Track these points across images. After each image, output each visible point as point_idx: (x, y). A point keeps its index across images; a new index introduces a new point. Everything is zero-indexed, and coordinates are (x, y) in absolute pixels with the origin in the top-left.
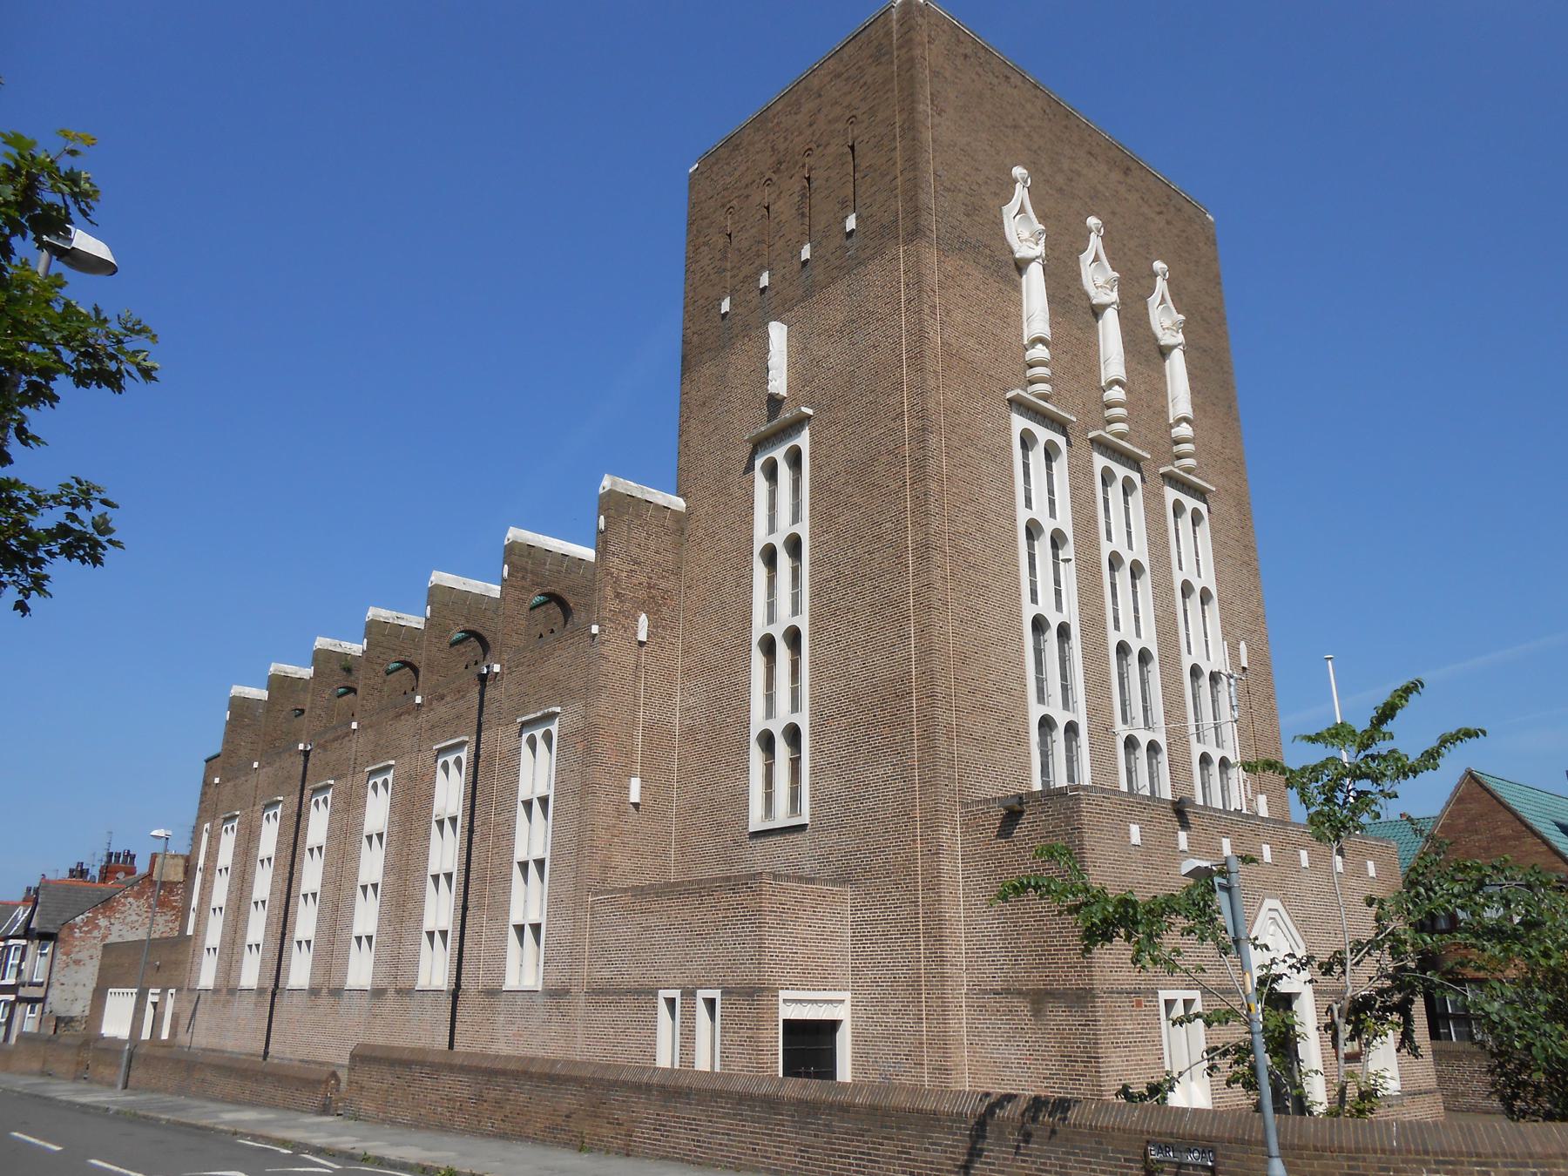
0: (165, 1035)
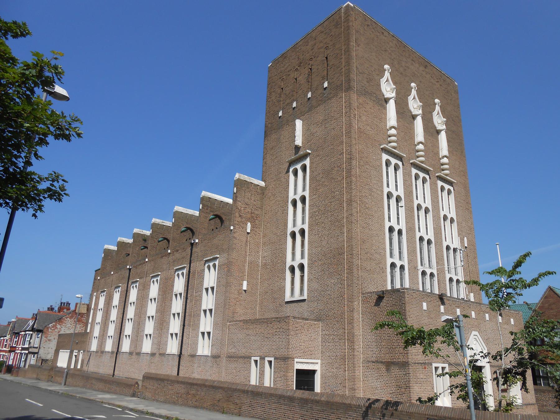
0: (79, 367)
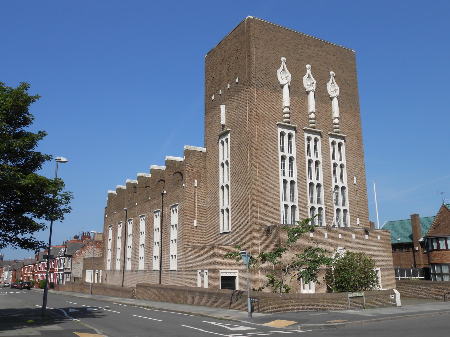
0: (100, 282)
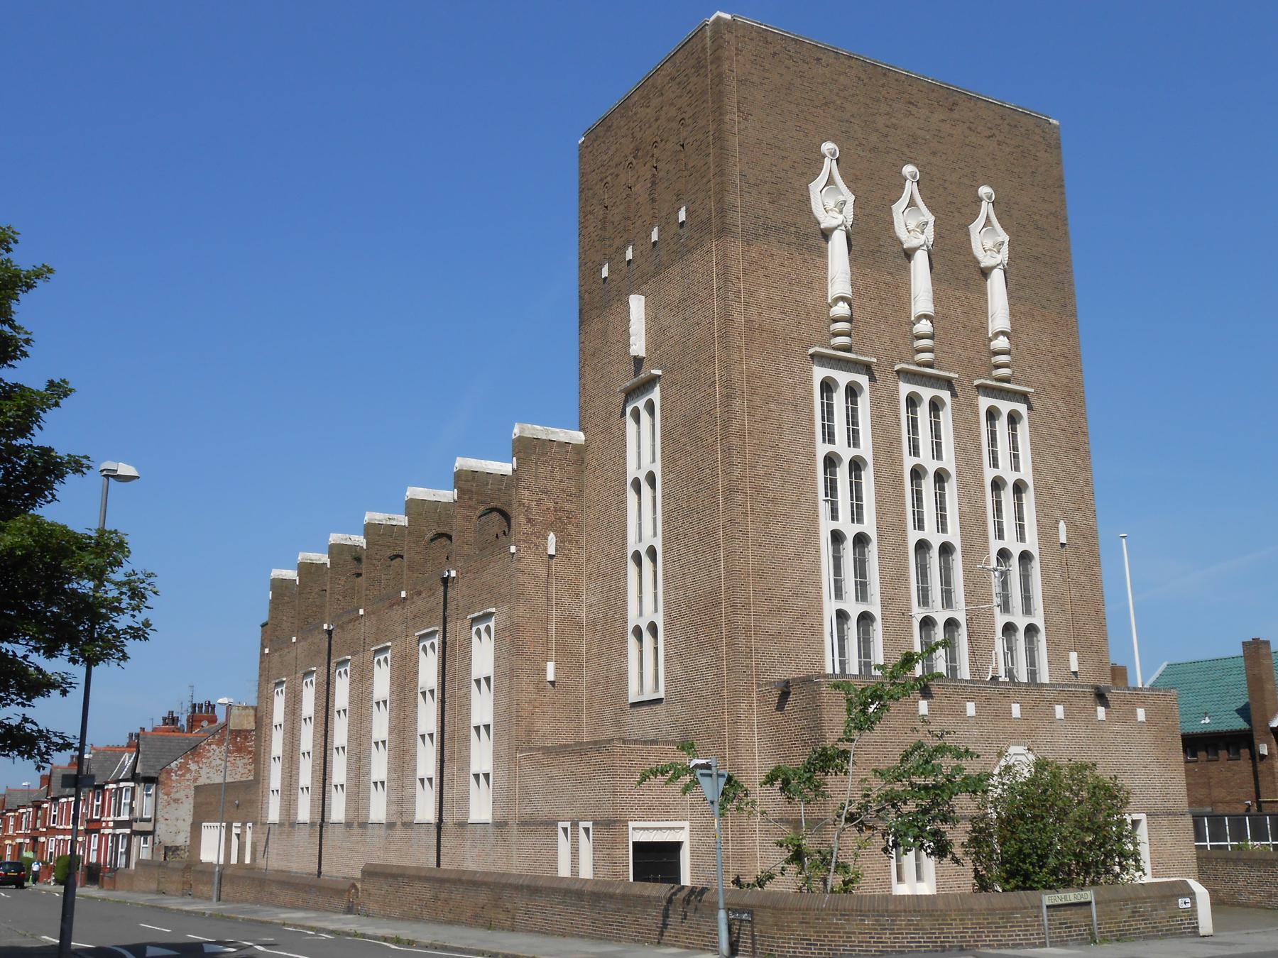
0: (248, 861)
